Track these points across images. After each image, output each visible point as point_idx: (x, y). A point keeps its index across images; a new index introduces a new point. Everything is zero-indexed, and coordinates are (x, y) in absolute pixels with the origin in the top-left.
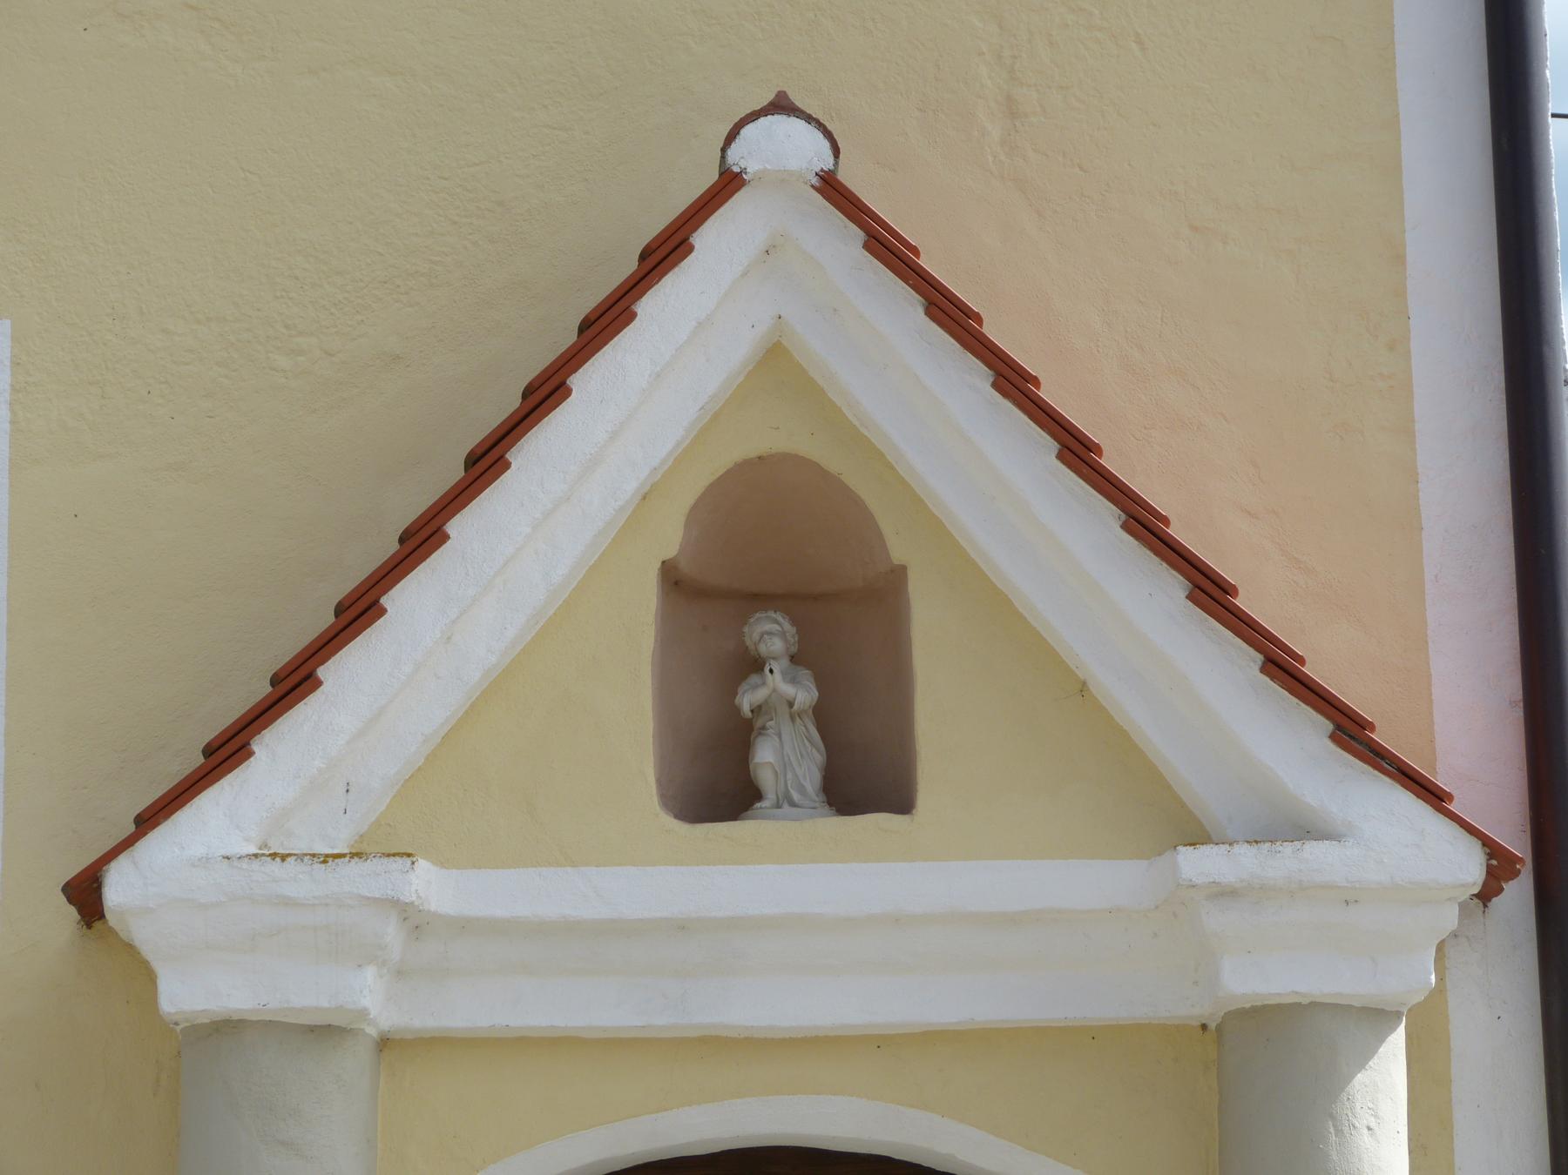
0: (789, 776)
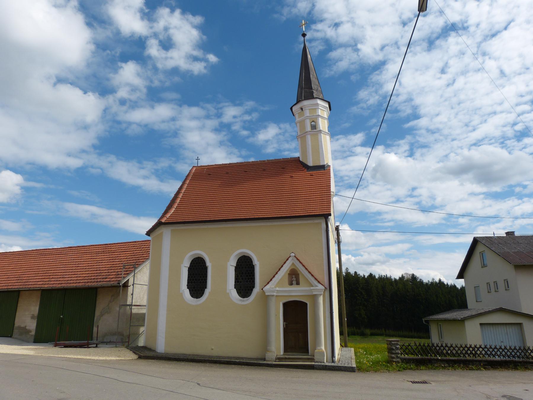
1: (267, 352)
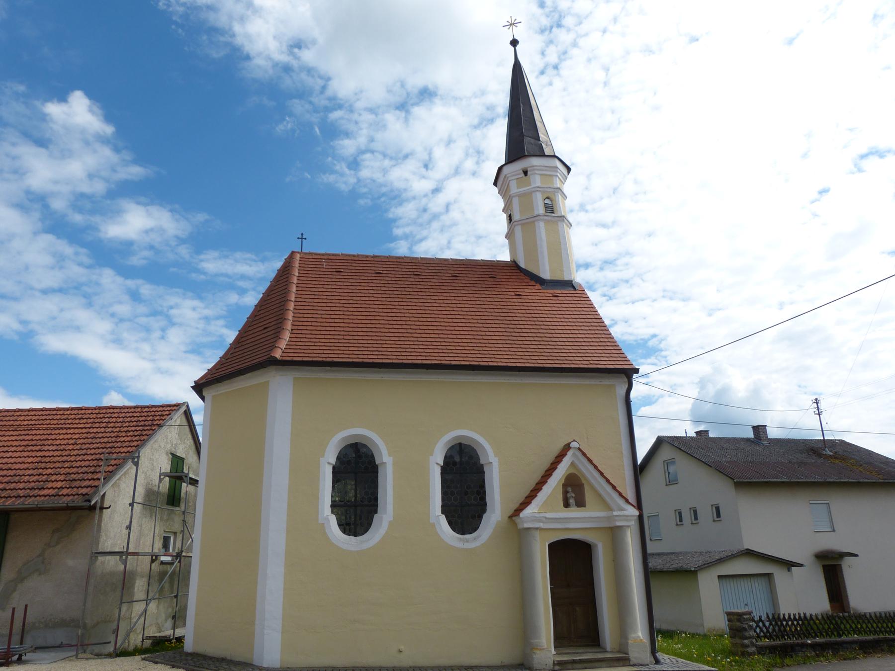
1: (535, 651)
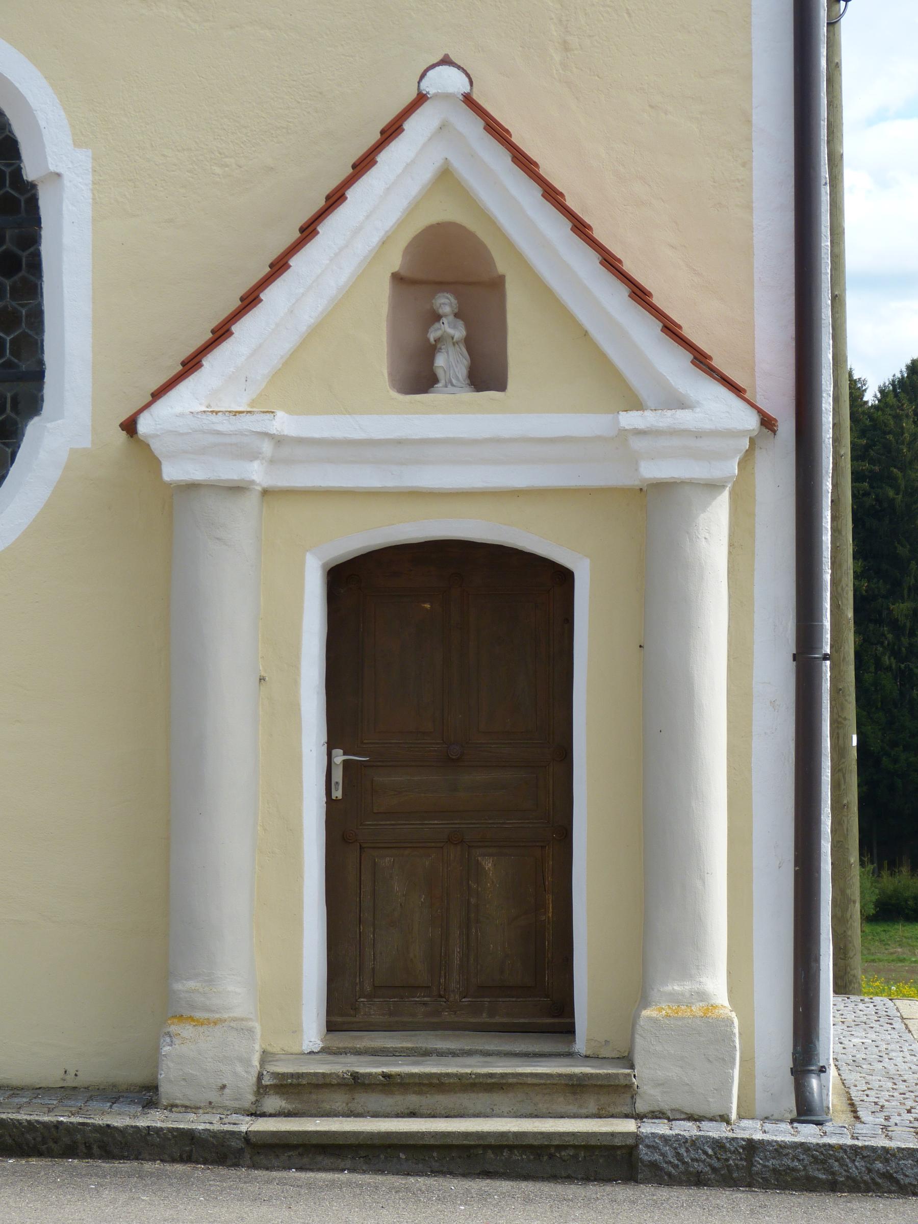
0: (452, 371)
1: (173, 1029)
